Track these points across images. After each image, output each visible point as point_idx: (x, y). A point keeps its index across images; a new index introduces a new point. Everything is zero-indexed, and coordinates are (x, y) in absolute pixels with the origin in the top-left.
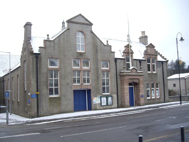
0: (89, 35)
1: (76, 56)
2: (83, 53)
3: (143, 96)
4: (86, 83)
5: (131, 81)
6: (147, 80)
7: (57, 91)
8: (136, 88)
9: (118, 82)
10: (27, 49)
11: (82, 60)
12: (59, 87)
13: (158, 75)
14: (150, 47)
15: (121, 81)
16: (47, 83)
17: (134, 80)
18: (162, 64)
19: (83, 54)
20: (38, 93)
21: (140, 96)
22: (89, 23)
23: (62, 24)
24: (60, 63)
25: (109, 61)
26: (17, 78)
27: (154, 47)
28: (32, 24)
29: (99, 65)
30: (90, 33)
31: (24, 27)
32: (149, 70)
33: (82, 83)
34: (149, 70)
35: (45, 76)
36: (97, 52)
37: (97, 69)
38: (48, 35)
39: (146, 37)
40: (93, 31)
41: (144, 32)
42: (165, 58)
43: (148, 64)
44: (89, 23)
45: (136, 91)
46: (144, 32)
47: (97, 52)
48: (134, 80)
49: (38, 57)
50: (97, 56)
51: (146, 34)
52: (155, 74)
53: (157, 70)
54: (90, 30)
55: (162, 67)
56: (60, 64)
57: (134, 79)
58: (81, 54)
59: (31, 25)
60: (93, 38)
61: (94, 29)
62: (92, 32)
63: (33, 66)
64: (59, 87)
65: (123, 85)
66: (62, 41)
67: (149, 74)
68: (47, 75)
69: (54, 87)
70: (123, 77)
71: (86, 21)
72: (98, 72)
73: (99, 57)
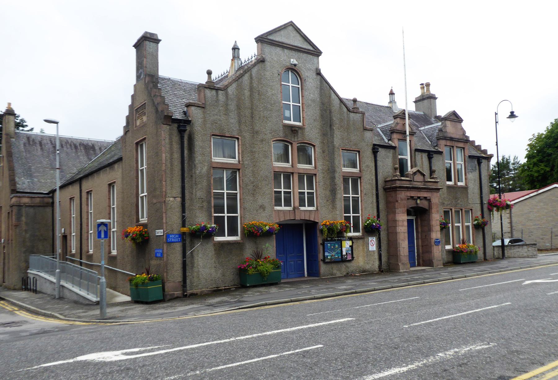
0: (311, 82)
1: (281, 134)
2: (299, 127)
3: (439, 242)
4: (305, 206)
5: (412, 204)
6: (446, 203)
7: (549, 181)
8: (421, 220)
9: (381, 206)
10: (149, 109)
11: (295, 145)
12: (238, 215)
13: (470, 191)
14: (452, 121)
15: (388, 203)
16: (209, 202)
17: (418, 201)
18: (479, 163)
19: (300, 131)
20: (185, 229)
21: (433, 241)
22: (312, 49)
23: (231, 52)
24: (242, 152)
25: (359, 152)
26: (109, 191)
27: (460, 120)
28: (159, 38)
29: (336, 162)
30: (314, 75)
31: (136, 46)
32: (449, 179)
33: (297, 204)
34: (449, 179)
35: (205, 183)
36: (331, 126)
37: (331, 171)
38: (209, 73)
39: (433, 98)
40: (323, 72)
41: (428, 85)
42: (482, 149)
43: (276, 192)
44: (312, 49)
45: (420, 230)
46: (428, 85)
47: (331, 126)
48: (418, 201)
49: (185, 131)
50: (332, 136)
51: (433, 91)
52: (462, 187)
53: (466, 179)
54: (314, 68)
55: (477, 171)
56: (242, 154)
57: (419, 198)
58: (293, 130)
59: (157, 41)
60: (321, 89)
61: (325, 65)
62: (319, 73)
63: (172, 154)
64: (238, 215)
65: (394, 213)
66: (247, 93)
67: (449, 187)
68: (210, 181)
69: (226, 215)
70: (393, 194)
71: (306, 43)
72: (333, 178)
73: (337, 142)
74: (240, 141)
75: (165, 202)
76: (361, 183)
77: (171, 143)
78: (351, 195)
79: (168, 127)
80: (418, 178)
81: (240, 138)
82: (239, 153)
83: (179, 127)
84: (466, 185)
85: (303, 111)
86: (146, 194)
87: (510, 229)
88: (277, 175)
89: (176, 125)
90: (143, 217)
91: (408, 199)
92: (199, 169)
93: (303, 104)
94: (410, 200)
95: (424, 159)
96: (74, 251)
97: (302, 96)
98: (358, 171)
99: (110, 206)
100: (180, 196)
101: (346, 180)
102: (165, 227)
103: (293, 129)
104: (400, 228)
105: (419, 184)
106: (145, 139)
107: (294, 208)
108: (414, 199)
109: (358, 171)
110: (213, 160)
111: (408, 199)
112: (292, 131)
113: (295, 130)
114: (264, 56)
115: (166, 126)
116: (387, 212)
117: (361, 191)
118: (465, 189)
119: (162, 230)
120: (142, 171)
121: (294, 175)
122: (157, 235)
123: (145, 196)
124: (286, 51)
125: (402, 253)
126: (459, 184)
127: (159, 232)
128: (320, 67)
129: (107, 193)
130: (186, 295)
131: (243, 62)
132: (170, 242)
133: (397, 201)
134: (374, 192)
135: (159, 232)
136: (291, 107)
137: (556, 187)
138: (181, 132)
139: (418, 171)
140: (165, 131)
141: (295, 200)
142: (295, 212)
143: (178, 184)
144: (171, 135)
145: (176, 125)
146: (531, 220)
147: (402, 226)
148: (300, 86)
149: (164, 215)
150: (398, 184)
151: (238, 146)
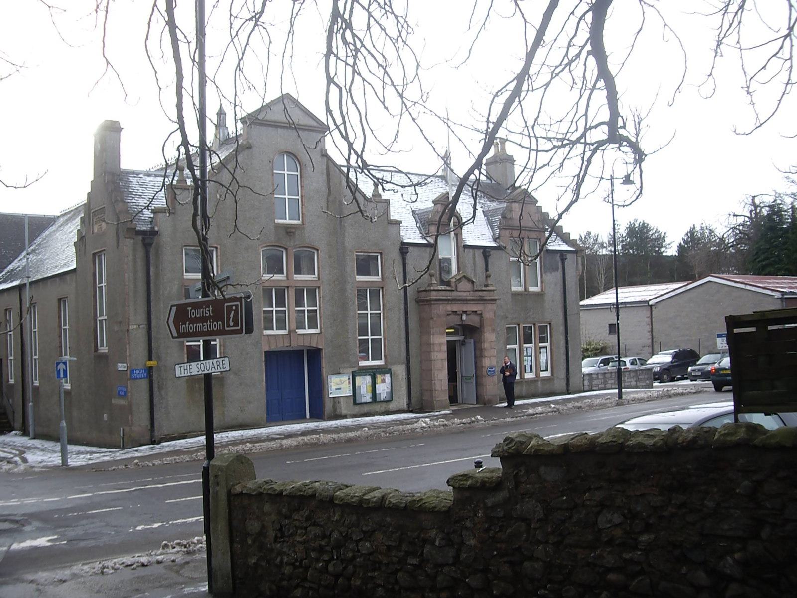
5: (455, 320)
6: (510, 316)
13: (548, 298)
17: (464, 317)
19: (297, 233)
20: (152, 362)
28: (122, 127)
33: (294, 326)
37: (341, 281)
49: (151, 244)
52: (536, 294)
53: (542, 282)
57: (465, 312)
58: (289, 230)
65: (429, 334)
72: (343, 290)
74: (219, 250)
75: (128, 331)
76: (383, 295)
77: (135, 261)
78: (369, 312)
79: (132, 241)
80: (464, 285)
81: (218, 247)
82: (217, 266)
83: (144, 240)
84: (542, 290)
85: (302, 205)
86: (106, 318)
87: (650, 341)
88: (267, 292)
89: (140, 237)
90: (102, 345)
91: (448, 315)
92: (168, 289)
93: (302, 197)
94: (452, 317)
95: (477, 259)
96: (12, 381)
97: (302, 187)
98: (380, 280)
99: (60, 327)
100: (146, 323)
101: (361, 294)
102: (128, 361)
103: (289, 230)
104: (436, 354)
105: (465, 294)
106: (104, 250)
107: (290, 331)
108: (459, 315)
109: (380, 280)
110: (185, 277)
111: (448, 315)
112: (287, 233)
113: (291, 232)
114: (250, 141)
115: (129, 240)
116: (421, 333)
117: (383, 305)
118: (540, 295)
119: (125, 365)
120: (101, 288)
121: (290, 288)
122: (119, 369)
123: (105, 320)
124: (280, 130)
125: (438, 387)
126: (532, 289)
127: (121, 367)
128: (326, 148)
129: (57, 309)
130: (155, 441)
131: (230, 133)
132: (134, 379)
133: (432, 319)
134: (403, 307)
135: (121, 367)
136: (288, 200)
137: (710, 281)
138: (147, 246)
139: (464, 276)
140: (128, 244)
141: (291, 320)
142: (290, 336)
143: (142, 309)
144: (134, 250)
145: (140, 237)
146: (678, 328)
147: (440, 351)
148: (298, 174)
149: (127, 347)
150: (434, 295)
151: (217, 257)
